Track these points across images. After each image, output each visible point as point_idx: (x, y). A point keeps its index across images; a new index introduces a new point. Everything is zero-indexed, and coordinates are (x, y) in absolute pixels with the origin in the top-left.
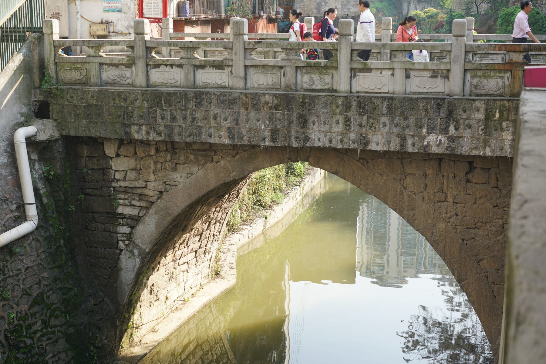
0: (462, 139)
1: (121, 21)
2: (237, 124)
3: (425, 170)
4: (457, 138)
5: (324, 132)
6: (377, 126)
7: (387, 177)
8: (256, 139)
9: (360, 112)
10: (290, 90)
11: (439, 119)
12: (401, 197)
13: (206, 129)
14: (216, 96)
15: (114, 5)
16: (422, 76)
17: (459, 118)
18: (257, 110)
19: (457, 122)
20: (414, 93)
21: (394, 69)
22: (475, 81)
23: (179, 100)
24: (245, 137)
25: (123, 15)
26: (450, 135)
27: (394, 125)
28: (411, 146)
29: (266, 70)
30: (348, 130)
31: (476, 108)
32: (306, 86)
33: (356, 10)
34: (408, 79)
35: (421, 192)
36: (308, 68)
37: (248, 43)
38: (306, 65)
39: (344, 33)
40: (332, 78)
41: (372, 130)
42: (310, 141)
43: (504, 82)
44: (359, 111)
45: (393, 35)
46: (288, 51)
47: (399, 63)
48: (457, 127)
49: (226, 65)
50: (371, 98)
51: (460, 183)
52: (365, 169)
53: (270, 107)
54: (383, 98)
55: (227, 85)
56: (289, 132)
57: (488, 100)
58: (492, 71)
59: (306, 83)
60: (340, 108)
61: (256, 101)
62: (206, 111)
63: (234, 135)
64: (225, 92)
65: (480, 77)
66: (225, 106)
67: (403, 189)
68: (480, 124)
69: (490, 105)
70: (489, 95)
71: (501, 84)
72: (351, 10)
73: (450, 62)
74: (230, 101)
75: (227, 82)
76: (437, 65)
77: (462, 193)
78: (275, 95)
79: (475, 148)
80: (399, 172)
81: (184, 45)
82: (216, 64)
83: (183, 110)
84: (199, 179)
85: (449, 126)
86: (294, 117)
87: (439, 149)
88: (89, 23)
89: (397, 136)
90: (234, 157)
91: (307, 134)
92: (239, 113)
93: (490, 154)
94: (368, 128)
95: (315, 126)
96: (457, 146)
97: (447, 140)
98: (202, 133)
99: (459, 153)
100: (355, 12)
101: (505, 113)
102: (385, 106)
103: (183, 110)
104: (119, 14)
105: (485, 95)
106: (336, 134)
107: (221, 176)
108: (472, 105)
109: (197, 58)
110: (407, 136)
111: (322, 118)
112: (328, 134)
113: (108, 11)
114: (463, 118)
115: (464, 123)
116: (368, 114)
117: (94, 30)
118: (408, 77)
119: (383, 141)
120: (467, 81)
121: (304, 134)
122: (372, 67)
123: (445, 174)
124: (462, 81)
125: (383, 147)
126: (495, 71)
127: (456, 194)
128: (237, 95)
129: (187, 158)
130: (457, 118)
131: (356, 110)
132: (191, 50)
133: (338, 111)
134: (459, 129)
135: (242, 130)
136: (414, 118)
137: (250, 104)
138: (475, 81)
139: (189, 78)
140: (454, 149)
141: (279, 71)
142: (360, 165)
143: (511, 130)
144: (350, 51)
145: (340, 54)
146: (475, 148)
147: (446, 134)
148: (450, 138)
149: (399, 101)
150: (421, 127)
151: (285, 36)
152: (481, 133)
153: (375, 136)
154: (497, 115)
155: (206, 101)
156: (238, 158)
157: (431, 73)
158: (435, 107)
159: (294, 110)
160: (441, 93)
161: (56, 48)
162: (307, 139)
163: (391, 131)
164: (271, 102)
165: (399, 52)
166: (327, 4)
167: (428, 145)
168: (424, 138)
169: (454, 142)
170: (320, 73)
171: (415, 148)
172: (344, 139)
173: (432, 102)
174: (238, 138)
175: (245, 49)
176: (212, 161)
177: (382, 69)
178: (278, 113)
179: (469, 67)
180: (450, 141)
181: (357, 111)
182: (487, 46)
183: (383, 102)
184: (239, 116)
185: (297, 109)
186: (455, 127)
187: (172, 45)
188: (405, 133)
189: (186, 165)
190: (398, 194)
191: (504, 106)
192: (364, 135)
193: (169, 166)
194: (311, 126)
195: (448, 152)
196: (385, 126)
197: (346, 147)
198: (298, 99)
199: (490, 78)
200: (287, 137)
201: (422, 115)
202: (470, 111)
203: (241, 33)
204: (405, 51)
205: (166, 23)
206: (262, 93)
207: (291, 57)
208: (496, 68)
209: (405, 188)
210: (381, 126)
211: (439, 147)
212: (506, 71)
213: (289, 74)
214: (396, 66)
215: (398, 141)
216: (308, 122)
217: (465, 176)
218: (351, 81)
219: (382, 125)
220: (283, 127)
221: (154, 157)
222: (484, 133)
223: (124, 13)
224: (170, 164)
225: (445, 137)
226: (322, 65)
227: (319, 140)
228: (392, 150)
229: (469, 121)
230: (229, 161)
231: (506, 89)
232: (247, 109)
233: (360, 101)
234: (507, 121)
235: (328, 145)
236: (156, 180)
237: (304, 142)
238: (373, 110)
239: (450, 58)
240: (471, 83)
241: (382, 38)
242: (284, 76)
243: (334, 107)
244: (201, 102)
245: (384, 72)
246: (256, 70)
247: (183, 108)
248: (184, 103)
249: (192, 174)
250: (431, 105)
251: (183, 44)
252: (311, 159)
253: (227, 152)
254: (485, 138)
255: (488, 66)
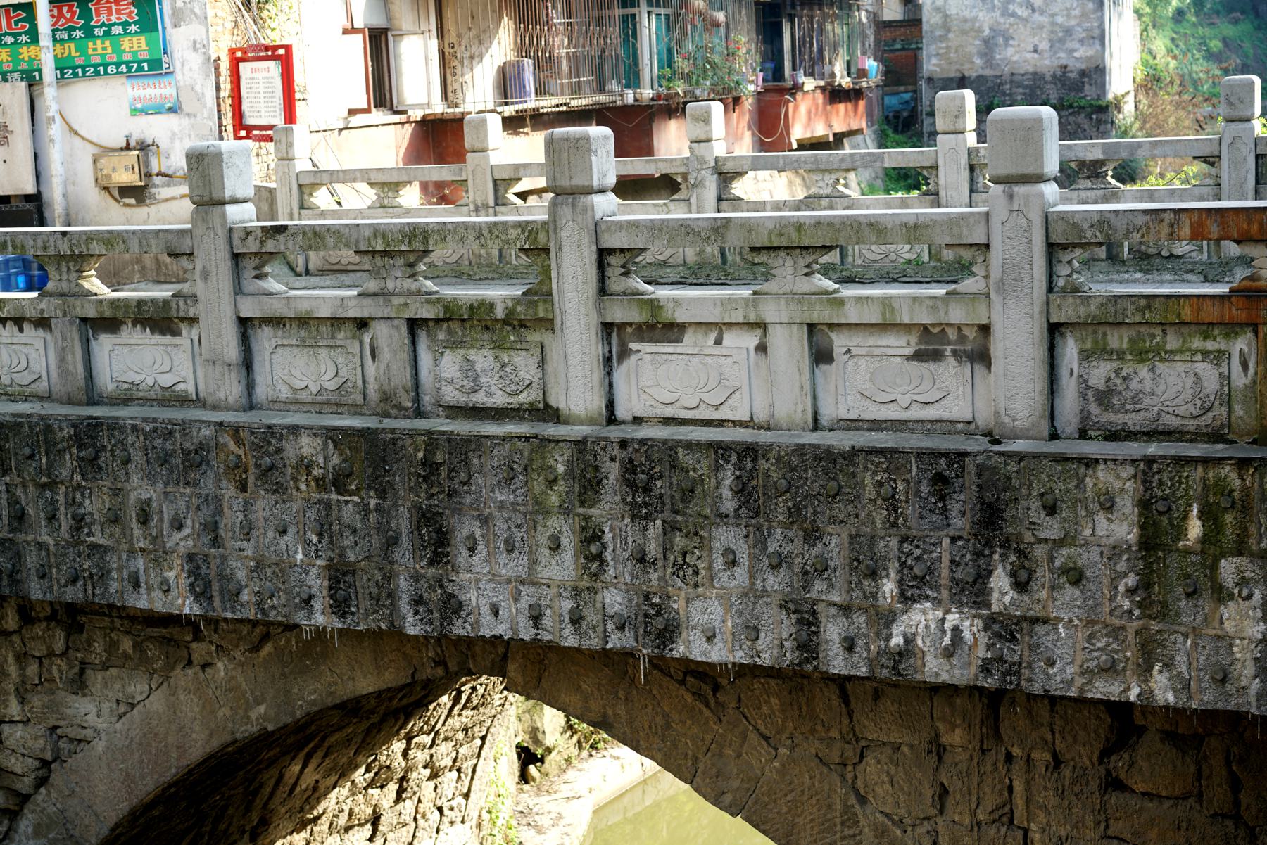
0: (1046, 628)
1: (181, 139)
2: (216, 542)
3: (936, 730)
4: (1025, 625)
5: (509, 582)
6: (701, 565)
7: (792, 749)
8: (283, 601)
9: (634, 504)
10: (394, 412)
11: (946, 542)
12: (847, 832)
13: (120, 558)
14: (142, 438)
15: (158, 91)
16: (877, 351)
17: (1028, 538)
18: (276, 491)
19: (1022, 554)
20: (852, 425)
21: (762, 326)
22: (1099, 373)
23: (27, 451)
24: (246, 591)
25: (185, 121)
26: (995, 608)
27: (766, 561)
28: (841, 651)
29: (314, 333)
30: (595, 576)
31: (1098, 495)
32: (451, 395)
33: (1090, 53)
34: (823, 367)
35: (927, 819)
36: (455, 325)
37: (243, 234)
38: (441, 315)
39: (565, 183)
40: (542, 364)
41: (684, 580)
42: (464, 614)
43: (1226, 379)
44: (629, 499)
45: (977, 150)
46: (378, 258)
47: (783, 302)
48: (1023, 576)
49: (182, 319)
50: (670, 447)
51: (1077, 789)
52: (707, 712)
53: (317, 480)
54: (721, 449)
55: (191, 390)
56: (389, 577)
57: (1150, 461)
58: (1170, 331)
59: (451, 382)
60: (561, 487)
61: (270, 456)
62: (116, 492)
63: (208, 585)
64: (170, 422)
65: (1121, 355)
66: (172, 472)
67: (853, 800)
68: (1122, 566)
69: (1161, 483)
70: (1162, 433)
71: (1211, 381)
72: (1076, 55)
73: (988, 295)
74: (186, 453)
75: (192, 382)
76: (934, 308)
77: (1089, 834)
78: (333, 436)
79: (1103, 670)
80: (835, 734)
81: (45, 248)
82: (149, 311)
83: (44, 486)
84: (155, 723)
85: (990, 573)
86: (403, 522)
87: (953, 667)
88: (95, 150)
89: (781, 607)
90: (256, 648)
91: (451, 588)
92: (218, 500)
93: (1171, 697)
94: (669, 571)
95: (476, 559)
96: (1026, 658)
97: (986, 629)
98: (109, 572)
99: (1036, 688)
100: (1089, 59)
101: (1229, 518)
102: (728, 482)
103: (44, 486)
104: (172, 121)
105: (1144, 433)
106: (554, 590)
107: (220, 714)
108: (1081, 481)
109: (89, 293)
110: (820, 608)
111: (500, 527)
112: (526, 590)
113: (144, 112)
114: (1046, 540)
115: (1051, 559)
116: (667, 515)
117: (105, 172)
118: (822, 356)
119: (729, 624)
120: (1063, 373)
121: (441, 587)
122: (681, 317)
123: (1016, 751)
124: (1043, 372)
125: (732, 651)
126: (1185, 330)
127: (1063, 834)
128: (206, 432)
129: (113, 646)
130: (1020, 540)
131: (618, 498)
132: (71, 264)
133: (554, 499)
134: (1033, 586)
135: (232, 564)
136: (845, 536)
137: (252, 469)
138: (1099, 373)
139: (71, 368)
140: (1014, 670)
141: (354, 337)
142: (689, 698)
143: (1257, 595)
144: (594, 257)
145: (559, 267)
146: (1103, 670)
147: (977, 605)
148: (995, 621)
149: (779, 460)
150: (873, 574)
151: (629, 167)
152: (1126, 604)
153: (699, 604)
154: (1195, 529)
155: (112, 455)
156: (270, 654)
157: (914, 340)
158: (925, 488)
159: (401, 492)
160: (960, 426)
161: (306, 191)
162: (452, 606)
163: (759, 585)
164: (321, 461)
165: (783, 254)
166: (1011, 42)
167: (909, 647)
168: (886, 619)
169: (1013, 639)
170: (498, 346)
171: (856, 658)
172: (586, 612)
173: (914, 469)
174: (221, 593)
175: (236, 257)
176: (190, 663)
177: (720, 328)
178: (347, 502)
179: (1066, 311)
180: (1000, 636)
181: (624, 500)
182: (1141, 220)
183: (718, 468)
184: (219, 511)
185: (411, 488)
186: (1013, 574)
187: (10, 249)
188: (814, 595)
189: (113, 671)
190: (838, 821)
191: (1221, 487)
192: (656, 600)
193: (60, 672)
194: (462, 557)
195: (990, 682)
196: (733, 563)
197: (594, 642)
198: (411, 450)
199: (1162, 360)
200: (384, 595)
201: (874, 523)
202: (1075, 507)
203: (216, 195)
204: (806, 248)
205: (284, 140)
206: (288, 427)
207: (391, 285)
208: (1187, 314)
209: (863, 800)
210: (719, 564)
211: (954, 661)
212: (1232, 328)
213: (386, 349)
214: (771, 312)
215: (788, 627)
216: (452, 542)
217: (1101, 763)
218: (609, 373)
219: (720, 560)
220: (367, 558)
221: (16, 638)
222: (1140, 605)
223: (188, 115)
224: (64, 667)
225: (974, 616)
226: (500, 313)
227: (496, 612)
228: (768, 663)
229: (1072, 551)
230: (242, 665)
231: (1237, 407)
232: (244, 488)
233: (631, 461)
234: (1240, 554)
235: (526, 633)
236: (29, 720)
237: (443, 618)
238: (683, 501)
239: (987, 277)
240: (1083, 380)
241: (940, 163)
242: (374, 357)
243: (539, 485)
244: (96, 458)
245: (730, 339)
246: (280, 333)
247: (44, 479)
248: (44, 460)
249: (133, 706)
250: (908, 481)
251: (40, 244)
252: (512, 667)
253: (234, 631)
254: (1147, 629)
255: (1149, 307)
